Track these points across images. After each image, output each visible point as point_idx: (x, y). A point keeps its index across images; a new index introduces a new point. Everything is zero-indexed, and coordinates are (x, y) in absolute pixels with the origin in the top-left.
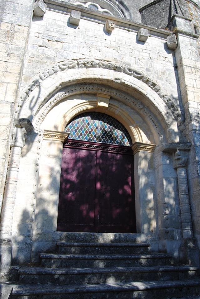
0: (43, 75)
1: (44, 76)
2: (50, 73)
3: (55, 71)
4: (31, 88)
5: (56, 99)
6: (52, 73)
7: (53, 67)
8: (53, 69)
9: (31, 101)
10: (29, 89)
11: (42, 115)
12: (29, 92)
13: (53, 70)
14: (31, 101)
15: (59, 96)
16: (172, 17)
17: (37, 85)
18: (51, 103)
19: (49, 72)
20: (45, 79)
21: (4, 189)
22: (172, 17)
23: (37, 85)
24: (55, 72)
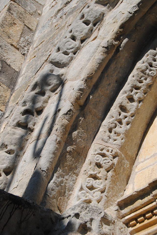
0: (61, 52)
1: (66, 53)
2: (79, 36)
3: (92, 19)
4: (33, 107)
5: (137, 88)
6: (86, 31)
7: (83, 16)
8: (83, 20)
9: (38, 139)
10: (27, 112)
11: (101, 160)
12: (26, 119)
13: (87, 23)
14: (38, 139)
15: (143, 72)
16: (156, 119)
17: (50, 88)
18: (123, 108)
19: (76, 34)
20: (72, 59)
21: (142, 147)
22: (156, 116)
23: (50, 88)
24: (95, 25)
